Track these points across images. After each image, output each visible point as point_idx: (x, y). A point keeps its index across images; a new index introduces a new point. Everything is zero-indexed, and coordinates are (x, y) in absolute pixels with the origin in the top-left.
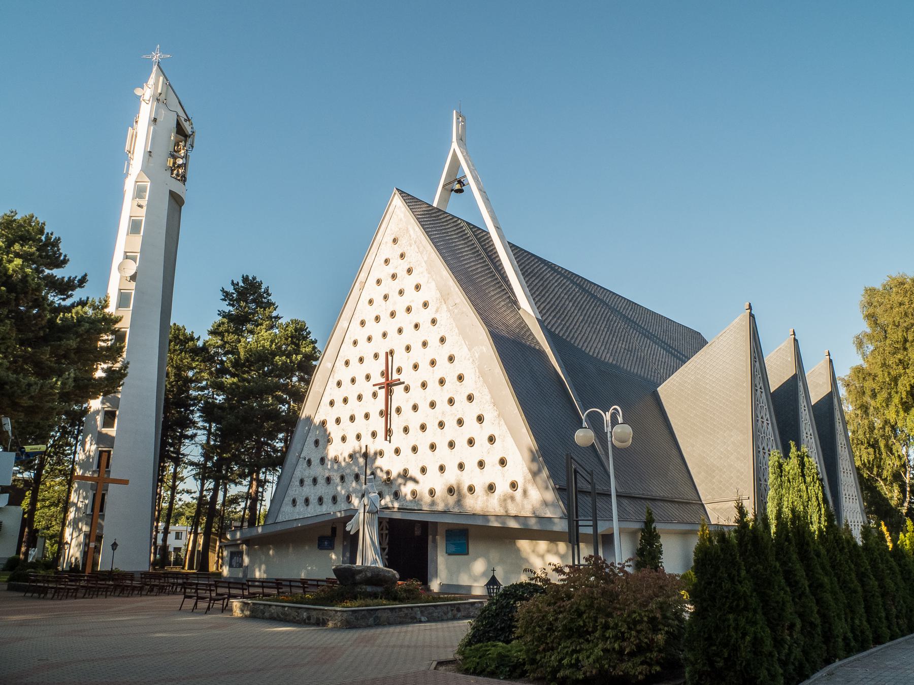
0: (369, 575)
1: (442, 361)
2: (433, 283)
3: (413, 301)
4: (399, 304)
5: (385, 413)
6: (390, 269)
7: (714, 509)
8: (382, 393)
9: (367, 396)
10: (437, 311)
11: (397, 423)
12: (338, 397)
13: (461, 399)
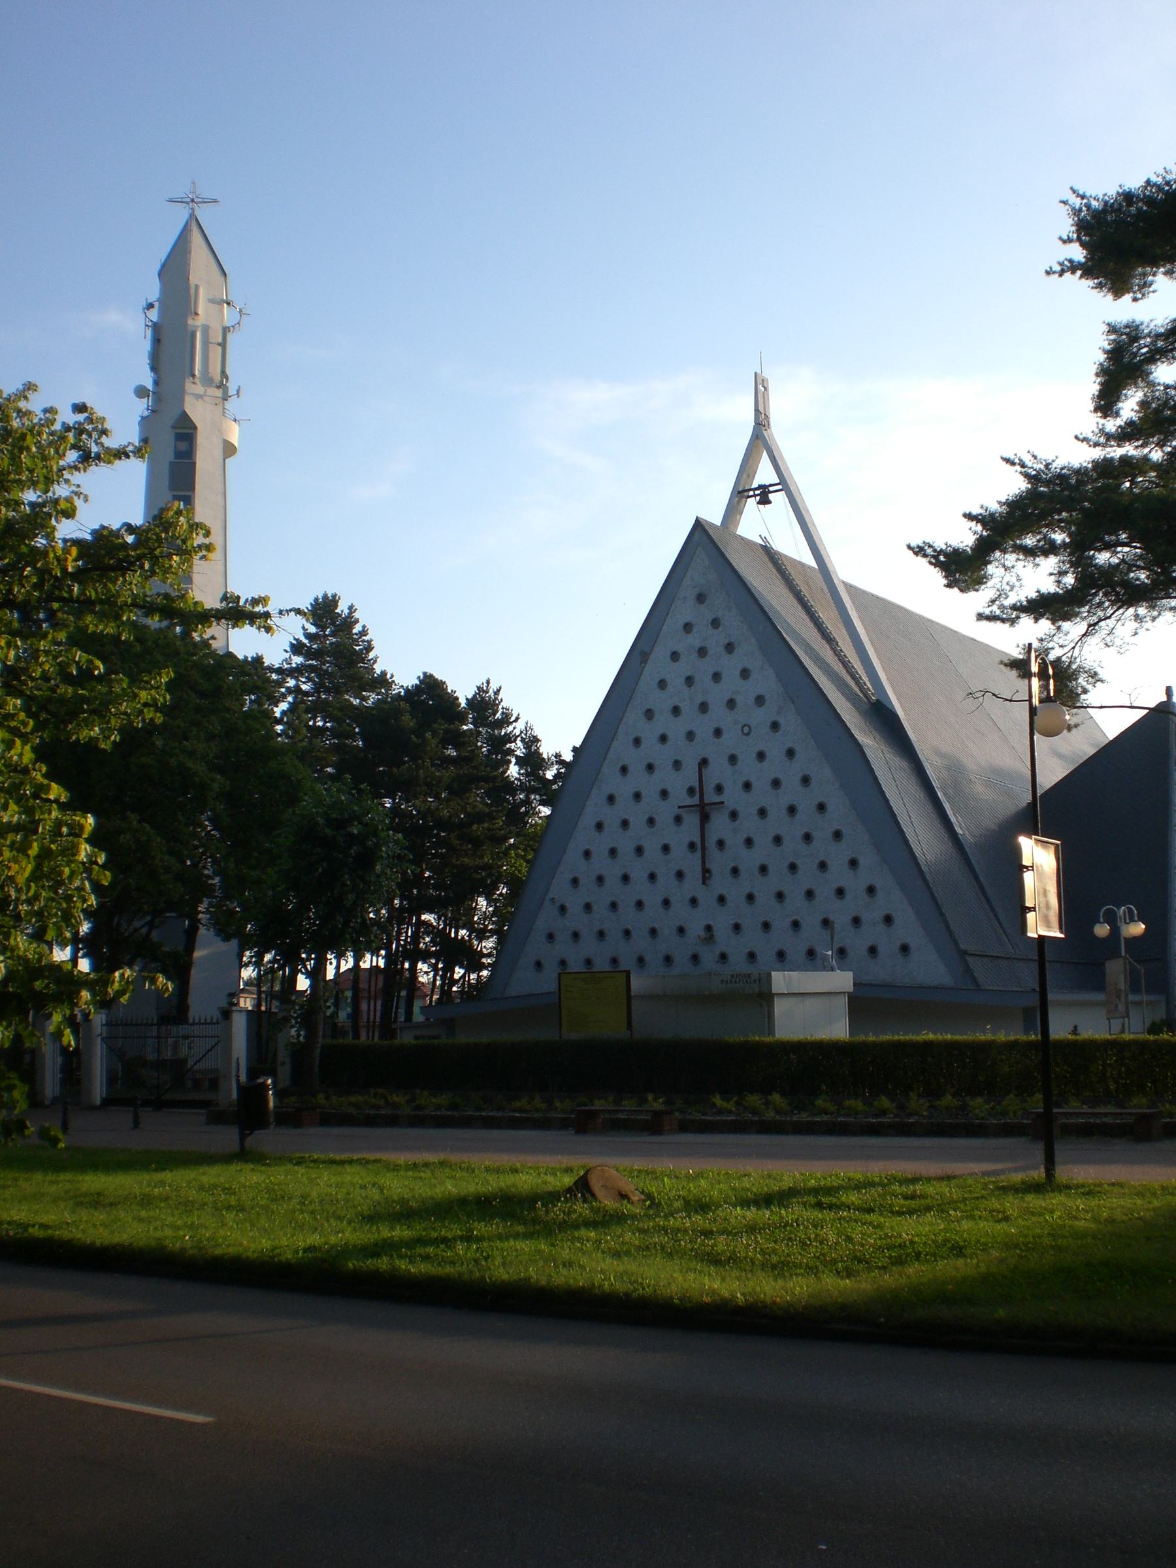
4: (717, 695)
10: (779, 713)
11: (719, 862)
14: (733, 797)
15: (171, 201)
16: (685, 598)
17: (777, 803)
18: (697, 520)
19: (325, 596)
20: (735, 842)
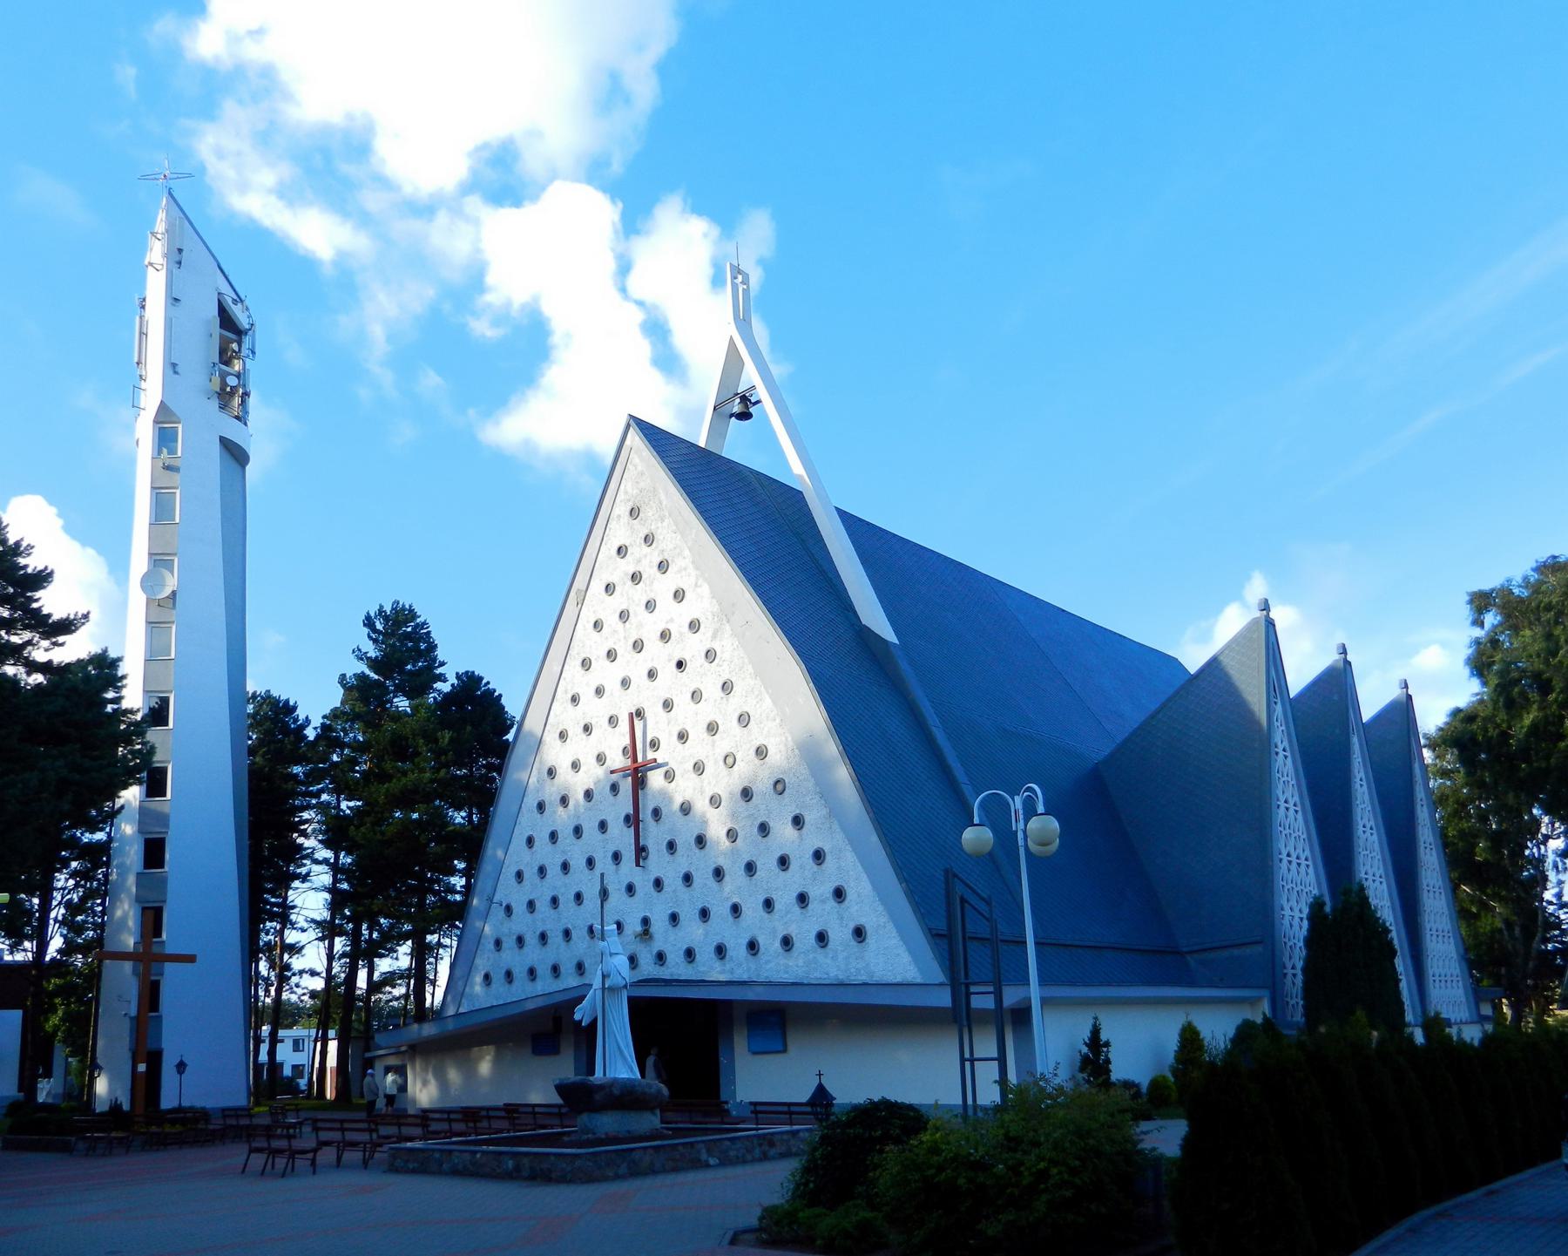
1: (729, 724)
3: (672, 620)
4: (647, 625)
6: (627, 566)
10: (714, 637)
15: (191, 959)
19: (287, 701)
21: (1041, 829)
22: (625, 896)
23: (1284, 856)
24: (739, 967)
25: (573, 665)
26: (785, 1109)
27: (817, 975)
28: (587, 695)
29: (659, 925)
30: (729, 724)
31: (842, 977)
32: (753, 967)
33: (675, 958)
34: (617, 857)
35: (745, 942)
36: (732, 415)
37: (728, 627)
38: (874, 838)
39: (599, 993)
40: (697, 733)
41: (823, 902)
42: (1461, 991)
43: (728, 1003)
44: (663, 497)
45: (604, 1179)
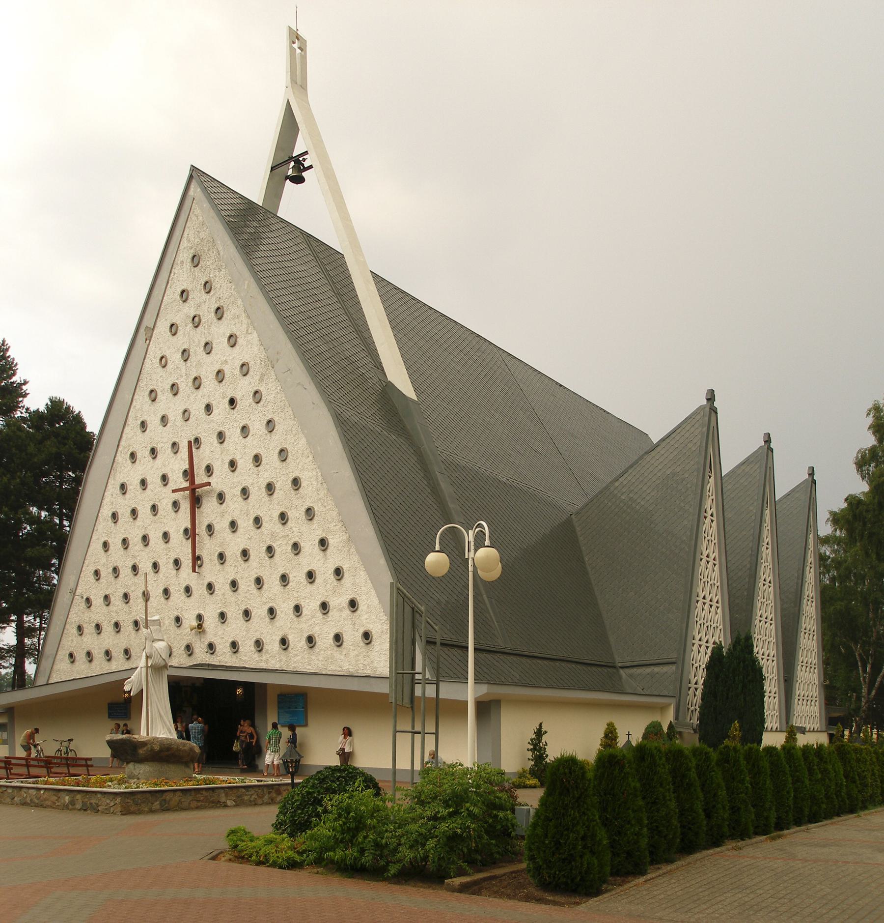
0: (157, 748)
1: (271, 458)
2: (255, 335)
3: (226, 362)
4: (206, 367)
5: (191, 534)
6: (189, 310)
7: (631, 676)
8: (185, 506)
9: (165, 506)
10: (261, 380)
11: (208, 548)
12: (123, 507)
13: (296, 514)
14: (221, 480)
16: (182, 262)
17: (256, 481)
18: (193, 169)
20: (220, 526)
21: (485, 558)
22: (183, 596)
23: (700, 598)
24: (273, 658)
25: (142, 397)
26: (84, 762)
27: (333, 667)
28: (154, 422)
29: (211, 622)
30: (271, 458)
31: (352, 670)
32: (284, 659)
33: (223, 648)
34: (177, 562)
35: (278, 638)
36: (287, 177)
37: (272, 373)
38: (382, 561)
39: (144, 670)
40: (245, 464)
41: (341, 610)
42: (817, 709)
43: (263, 686)
44: (220, 249)
45: (139, 812)
